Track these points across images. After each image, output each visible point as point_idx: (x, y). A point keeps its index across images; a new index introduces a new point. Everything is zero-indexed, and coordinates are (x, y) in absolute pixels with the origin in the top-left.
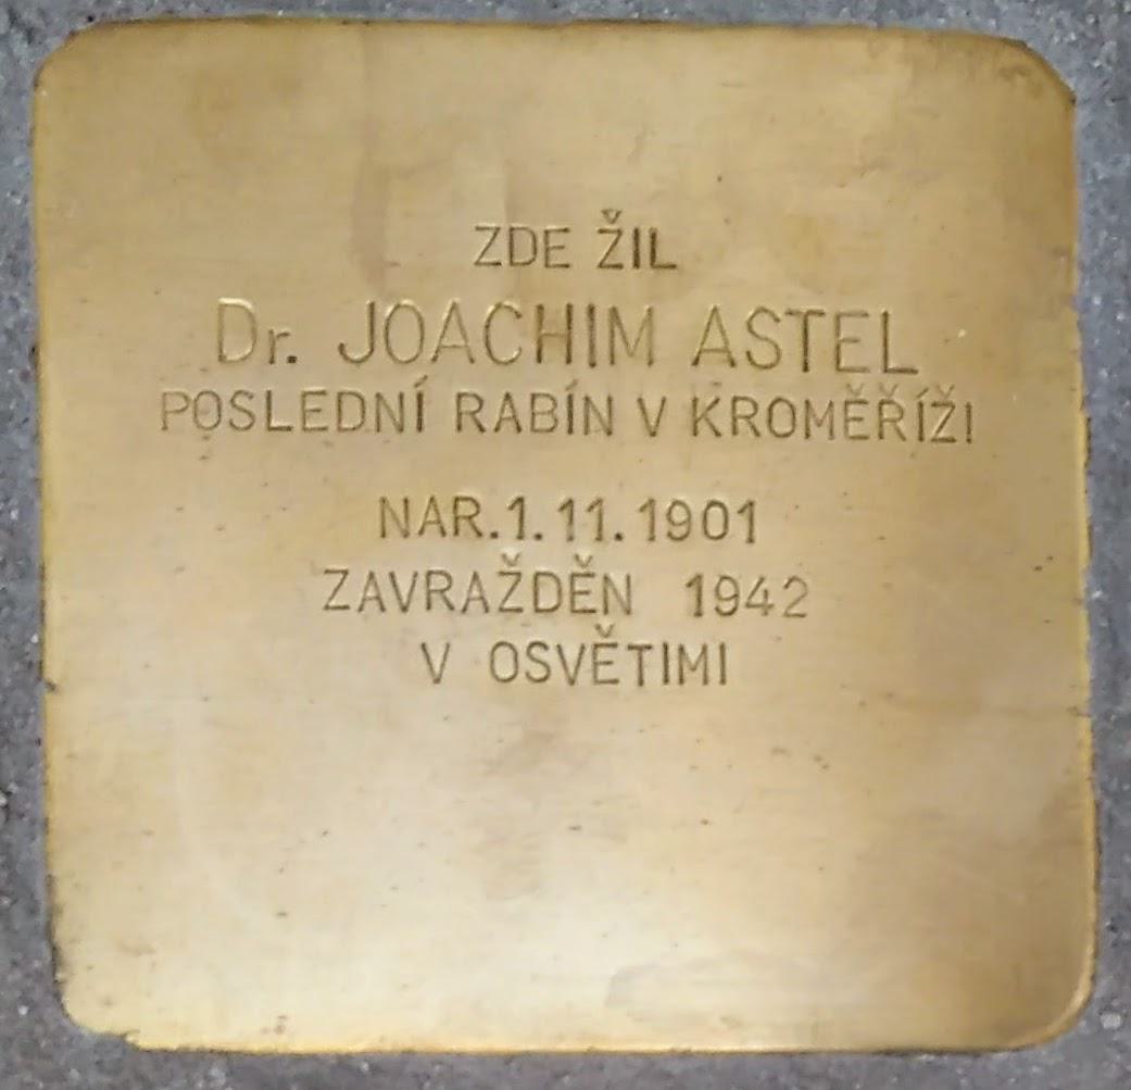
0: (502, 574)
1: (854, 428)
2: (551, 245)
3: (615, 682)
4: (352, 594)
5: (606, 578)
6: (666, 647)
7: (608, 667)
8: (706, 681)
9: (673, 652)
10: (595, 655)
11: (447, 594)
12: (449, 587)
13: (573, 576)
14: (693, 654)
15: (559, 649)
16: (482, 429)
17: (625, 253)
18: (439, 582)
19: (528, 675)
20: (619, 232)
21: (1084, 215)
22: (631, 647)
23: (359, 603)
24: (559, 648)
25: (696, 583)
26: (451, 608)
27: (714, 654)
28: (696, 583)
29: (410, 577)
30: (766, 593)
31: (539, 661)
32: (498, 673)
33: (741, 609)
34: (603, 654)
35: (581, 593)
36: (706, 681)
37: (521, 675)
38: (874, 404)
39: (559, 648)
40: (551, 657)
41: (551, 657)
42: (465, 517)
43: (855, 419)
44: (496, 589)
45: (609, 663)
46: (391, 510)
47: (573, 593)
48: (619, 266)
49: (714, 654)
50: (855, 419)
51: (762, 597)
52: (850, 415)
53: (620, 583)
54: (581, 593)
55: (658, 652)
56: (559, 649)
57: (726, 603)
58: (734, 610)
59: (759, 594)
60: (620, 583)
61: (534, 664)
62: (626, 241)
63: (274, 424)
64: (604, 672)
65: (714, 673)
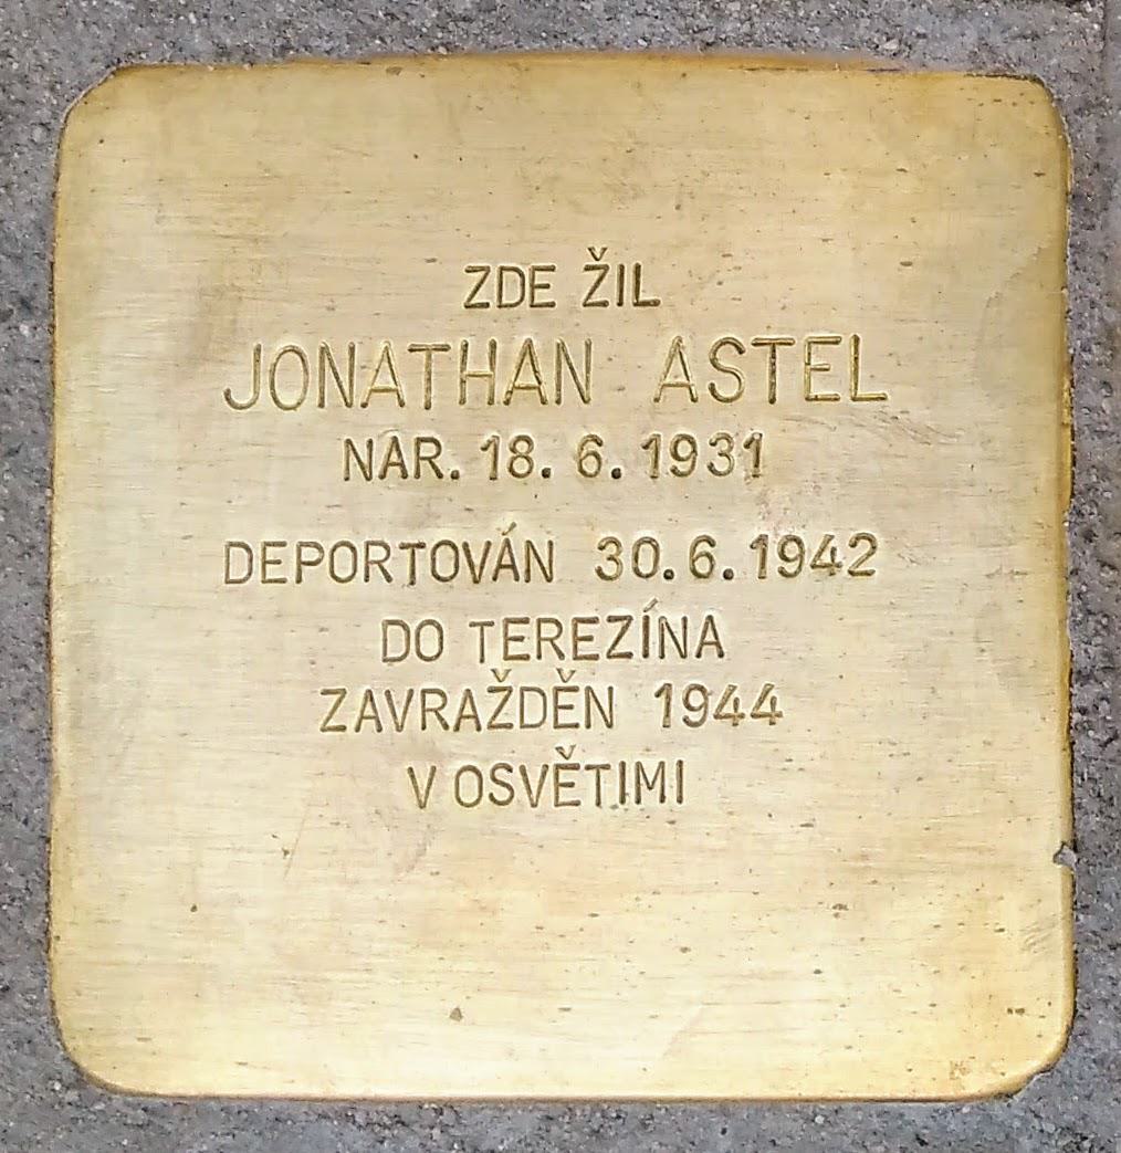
2: (536, 282)
3: (577, 804)
5: (589, 689)
7: (519, 644)
8: (663, 799)
10: (557, 775)
13: (558, 690)
15: (523, 771)
16: (440, 476)
17: (607, 291)
18: (434, 701)
19: (510, 770)
20: (606, 268)
26: (446, 727)
27: (671, 772)
28: (665, 691)
30: (736, 702)
32: (463, 799)
33: (710, 717)
34: (564, 776)
35: (540, 287)
36: (663, 799)
40: (515, 779)
41: (515, 779)
42: (375, 562)
44: (486, 707)
45: (571, 785)
47: (557, 707)
48: (605, 304)
49: (671, 772)
51: (769, 705)
54: (540, 287)
55: (616, 768)
56: (523, 771)
58: (703, 720)
59: (767, 703)
61: (498, 787)
62: (611, 279)
65: (671, 794)
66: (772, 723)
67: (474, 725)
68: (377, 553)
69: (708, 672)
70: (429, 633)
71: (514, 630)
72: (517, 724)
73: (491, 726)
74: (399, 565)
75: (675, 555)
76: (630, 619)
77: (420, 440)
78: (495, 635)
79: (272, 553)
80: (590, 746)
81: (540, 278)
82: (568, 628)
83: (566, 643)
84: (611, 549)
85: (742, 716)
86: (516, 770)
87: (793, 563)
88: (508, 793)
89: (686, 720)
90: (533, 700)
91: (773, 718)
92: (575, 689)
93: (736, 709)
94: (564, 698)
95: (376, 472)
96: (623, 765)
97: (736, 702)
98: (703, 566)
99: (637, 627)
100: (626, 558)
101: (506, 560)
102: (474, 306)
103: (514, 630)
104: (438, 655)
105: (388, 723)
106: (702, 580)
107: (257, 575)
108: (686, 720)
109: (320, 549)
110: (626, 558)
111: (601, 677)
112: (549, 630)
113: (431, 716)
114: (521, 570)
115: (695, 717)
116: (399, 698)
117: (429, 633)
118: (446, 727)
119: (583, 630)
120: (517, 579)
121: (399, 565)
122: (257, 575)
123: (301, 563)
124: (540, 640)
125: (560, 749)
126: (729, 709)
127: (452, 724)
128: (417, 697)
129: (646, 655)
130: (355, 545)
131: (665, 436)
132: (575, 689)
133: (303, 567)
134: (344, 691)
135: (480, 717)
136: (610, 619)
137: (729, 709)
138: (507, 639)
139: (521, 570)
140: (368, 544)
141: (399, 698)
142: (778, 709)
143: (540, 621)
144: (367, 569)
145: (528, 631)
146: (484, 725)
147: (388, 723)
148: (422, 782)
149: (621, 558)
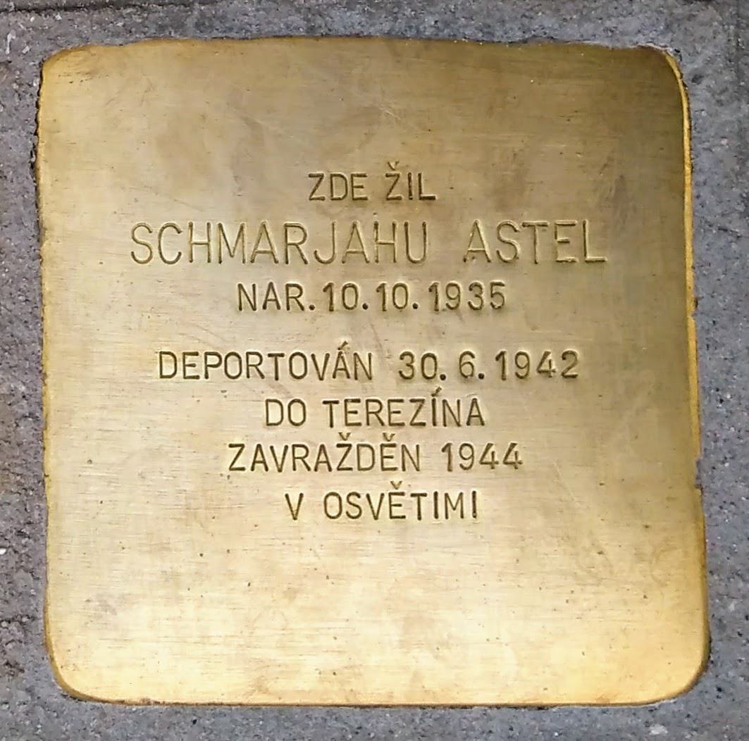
0: (339, 446)
1: (190, 371)
4: (245, 460)
5: (403, 446)
6: (436, 494)
9: (441, 498)
11: (306, 459)
12: (306, 456)
13: (382, 446)
14: (454, 498)
18: (300, 452)
19: (347, 513)
21: (520, 49)
22: (413, 495)
23: (251, 465)
24: (368, 496)
25: (447, 448)
26: (309, 469)
28: (447, 448)
29: (283, 449)
30: (516, 453)
31: (354, 505)
34: (395, 499)
37: (344, 514)
38: (202, 354)
39: (368, 496)
40: (362, 501)
43: (190, 365)
44: (335, 454)
46: (504, 358)
47: (383, 457)
50: (190, 365)
51: (514, 457)
52: (187, 362)
53: (412, 450)
55: (431, 498)
57: (466, 461)
60: (412, 450)
63: (335, 196)
64: (397, 511)
66: (493, 468)
67: (327, 467)
68: (254, 360)
69: (477, 438)
70: (296, 408)
71: (351, 407)
72: (355, 469)
73: (339, 469)
74: (267, 367)
75: (447, 362)
76: (423, 401)
77: (288, 286)
78: (338, 410)
79: (189, 359)
80: (410, 482)
81: (357, 182)
82: (385, 404)
83: (384, 416)
84: (407, 358)
85: (497, 463)
86: (364, 497)
87: (524, 369)
88: (358, 510)
89: (461, 466)
90: (366, 453)
91: (515, 465)
92: (394, 446)
93: (516, 458)
94: (386, 451)
95: (259, 305)
96: (436, 494)
97: (516, 453)
98: (467, 370)
99: (428, 405)
100: (417, 365)
101: (341, 366)
102: (313, 199)
103: (351, 407)
104: (304, 420)
105: (272, 466)
106: (407, 380)
107: (180, 373)
108: (461, 466)
109: (220, 357)
110: (417, 365)
111: (411, 438)
112: (374, 407)
113: (299, 462)
114: (351, 372)
115: (467, 463)
116: (279, 452)
117: (296, 408)
118: (309, 469)
119: (394, 407)
120: (348, 377)
121: (267, 367)
122: (180, 373)
123: (207, 366)
124: (368, 413)
125: (384, 435)
126: (511, 458)
127: (312, 467)
128: (290, 450)
129: (435, 424)
130: (240, 354)
131: (442, 283)
132: (394, 446)
133: (209, 369)
134: (242, 446)
135: (331, 462)
136: (412, 401)
137: (488, 458)
138: (346, 412)
139: (351, 372)
140: (248, 354)
141: (279, 452)
142: (520, 458)
143: (346, 401)
144: (248, 369)
145: (360, 408)
146: (334, 466)
147: (272, 466)
148: (294, 501)
149: (414, 364)
